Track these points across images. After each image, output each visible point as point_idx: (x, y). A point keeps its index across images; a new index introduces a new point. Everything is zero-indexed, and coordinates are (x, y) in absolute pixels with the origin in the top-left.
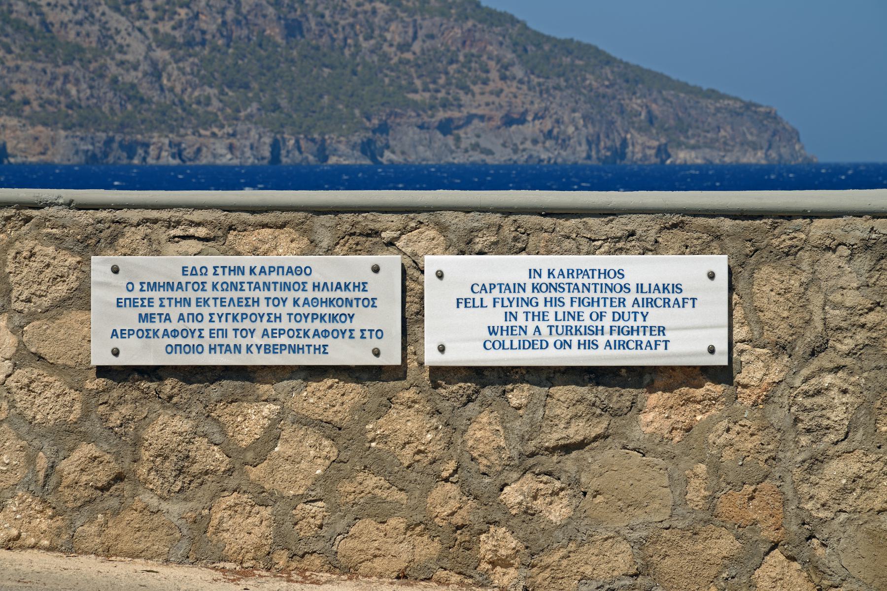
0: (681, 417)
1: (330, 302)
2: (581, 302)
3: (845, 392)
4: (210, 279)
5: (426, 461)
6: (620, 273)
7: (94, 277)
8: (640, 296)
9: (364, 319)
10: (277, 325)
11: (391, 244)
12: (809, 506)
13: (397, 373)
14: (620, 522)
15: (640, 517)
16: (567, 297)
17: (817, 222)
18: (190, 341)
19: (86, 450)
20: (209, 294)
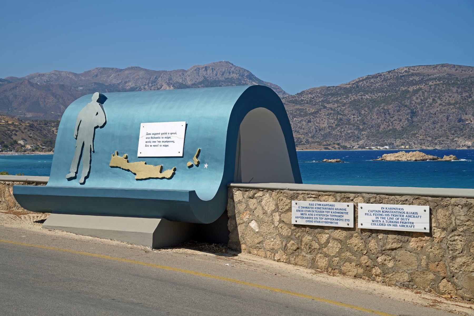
0: (420, 244)
1: (339, 213)
2: (393, 215)
3: (461, 241)
4: (314, 206)
5: (360, 250)
6: (402, 209)
7: (292, 205)
8: (407, 215)
9: (345, 217)
10: (328, 217)
11: (352, 200)
12: (452, 269)
13: (354, 229)
14: (405, 268)
15: (410, 267)
16: (390, 214)
17: (453, 199)
18: (310, 220)
19: (292, 242)
20: (314, 210)
